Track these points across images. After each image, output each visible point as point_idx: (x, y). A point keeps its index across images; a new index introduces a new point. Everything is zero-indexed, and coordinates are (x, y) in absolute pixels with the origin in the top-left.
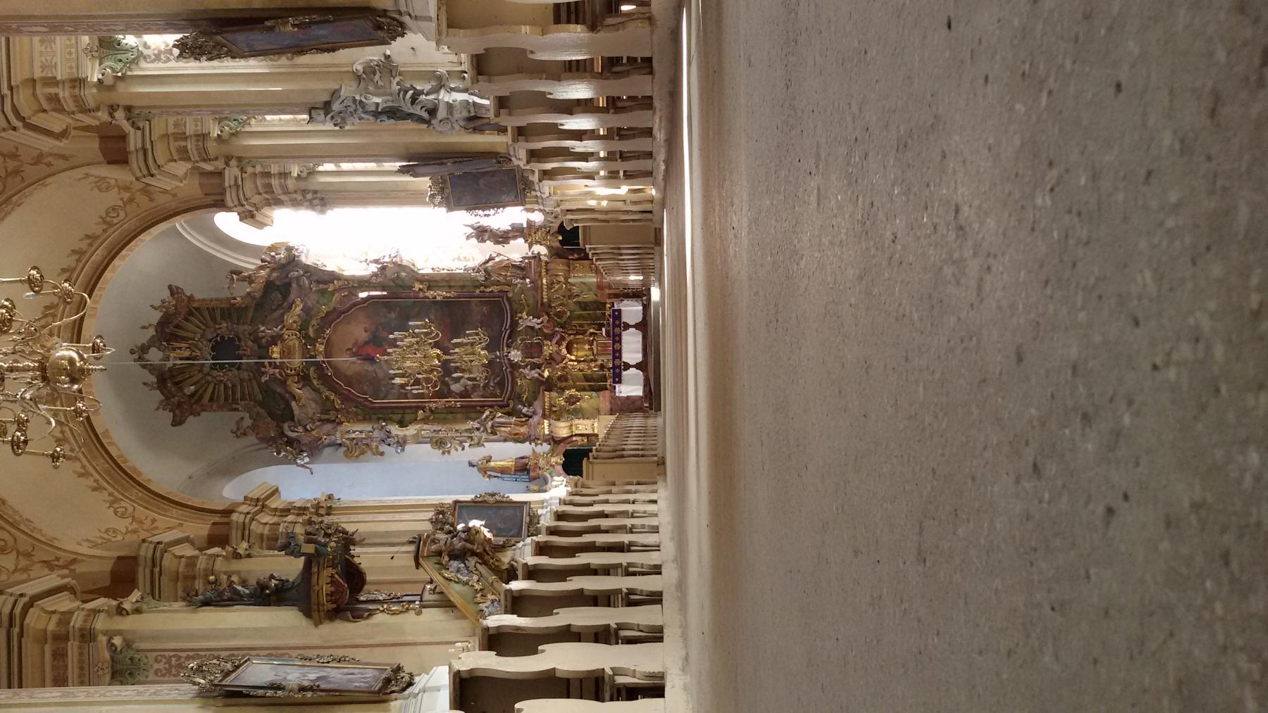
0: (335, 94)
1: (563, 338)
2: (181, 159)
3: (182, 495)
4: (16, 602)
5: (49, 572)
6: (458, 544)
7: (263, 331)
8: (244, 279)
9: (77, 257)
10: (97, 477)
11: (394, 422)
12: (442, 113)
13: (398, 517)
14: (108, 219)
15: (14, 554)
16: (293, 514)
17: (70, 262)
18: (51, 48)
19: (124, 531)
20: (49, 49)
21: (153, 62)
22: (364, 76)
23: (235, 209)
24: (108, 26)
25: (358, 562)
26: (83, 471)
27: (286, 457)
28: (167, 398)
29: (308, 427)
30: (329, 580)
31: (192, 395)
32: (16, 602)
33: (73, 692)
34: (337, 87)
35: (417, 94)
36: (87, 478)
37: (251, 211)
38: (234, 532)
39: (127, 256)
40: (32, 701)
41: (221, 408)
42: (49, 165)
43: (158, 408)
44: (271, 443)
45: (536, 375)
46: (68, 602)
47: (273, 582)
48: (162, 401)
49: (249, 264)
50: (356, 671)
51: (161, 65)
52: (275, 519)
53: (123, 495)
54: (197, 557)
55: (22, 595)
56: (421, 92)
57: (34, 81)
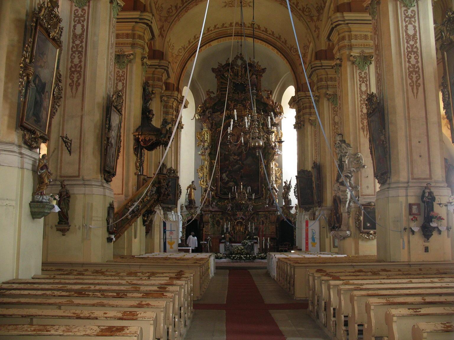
0: (349, 145)
1: (243, 219)
2: (318, 79)
3: (185, 72)
4: (150, 21)
5: (159, 28)
6: (163, 190)
7: (248, 102)
8: (268, 95)
9: (278, 37)
10: (194, 42)
11: (211, 151)
12: (342, 188)
13: (173, 154)
14: (293, 49)
15: (167, 16)
16: (176, 114)
17: (276, 35)
18: (363, 38)
19: (173, 52)
20: (362, 38)
21: (359, 76)
22: (356, 157)
23: (297, 95)
24: (379, 67)
25: (157, 148)
26: (196, 37)
27: (199, 110)
28: (223, 67)
29: (210, 118)
30: (151, 138)
31: (223, 75)
32: (150, 21)
33: (113, 47)
34: (351, 146)
35: (349, 178)
36: (193, 39)
37: (296, 101)
38: (170, 92)
39: (278, 55)
40: (111, 33)
41: (218, 86)
42: (315, 31)
43: (219, 63)
44: (204, 104)
45: (228, 208)
46: (148, 38)
47: (151, 116)
48: (221, 64)
49: (274, 97)
50: (114, 158)
51: (358, 78)
52: (174, 107)
53: (186, 52)
54: (162, 81)
55: (152, 22)
56: (350, 180)
57: (350, 32)
